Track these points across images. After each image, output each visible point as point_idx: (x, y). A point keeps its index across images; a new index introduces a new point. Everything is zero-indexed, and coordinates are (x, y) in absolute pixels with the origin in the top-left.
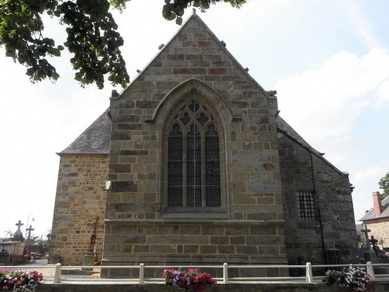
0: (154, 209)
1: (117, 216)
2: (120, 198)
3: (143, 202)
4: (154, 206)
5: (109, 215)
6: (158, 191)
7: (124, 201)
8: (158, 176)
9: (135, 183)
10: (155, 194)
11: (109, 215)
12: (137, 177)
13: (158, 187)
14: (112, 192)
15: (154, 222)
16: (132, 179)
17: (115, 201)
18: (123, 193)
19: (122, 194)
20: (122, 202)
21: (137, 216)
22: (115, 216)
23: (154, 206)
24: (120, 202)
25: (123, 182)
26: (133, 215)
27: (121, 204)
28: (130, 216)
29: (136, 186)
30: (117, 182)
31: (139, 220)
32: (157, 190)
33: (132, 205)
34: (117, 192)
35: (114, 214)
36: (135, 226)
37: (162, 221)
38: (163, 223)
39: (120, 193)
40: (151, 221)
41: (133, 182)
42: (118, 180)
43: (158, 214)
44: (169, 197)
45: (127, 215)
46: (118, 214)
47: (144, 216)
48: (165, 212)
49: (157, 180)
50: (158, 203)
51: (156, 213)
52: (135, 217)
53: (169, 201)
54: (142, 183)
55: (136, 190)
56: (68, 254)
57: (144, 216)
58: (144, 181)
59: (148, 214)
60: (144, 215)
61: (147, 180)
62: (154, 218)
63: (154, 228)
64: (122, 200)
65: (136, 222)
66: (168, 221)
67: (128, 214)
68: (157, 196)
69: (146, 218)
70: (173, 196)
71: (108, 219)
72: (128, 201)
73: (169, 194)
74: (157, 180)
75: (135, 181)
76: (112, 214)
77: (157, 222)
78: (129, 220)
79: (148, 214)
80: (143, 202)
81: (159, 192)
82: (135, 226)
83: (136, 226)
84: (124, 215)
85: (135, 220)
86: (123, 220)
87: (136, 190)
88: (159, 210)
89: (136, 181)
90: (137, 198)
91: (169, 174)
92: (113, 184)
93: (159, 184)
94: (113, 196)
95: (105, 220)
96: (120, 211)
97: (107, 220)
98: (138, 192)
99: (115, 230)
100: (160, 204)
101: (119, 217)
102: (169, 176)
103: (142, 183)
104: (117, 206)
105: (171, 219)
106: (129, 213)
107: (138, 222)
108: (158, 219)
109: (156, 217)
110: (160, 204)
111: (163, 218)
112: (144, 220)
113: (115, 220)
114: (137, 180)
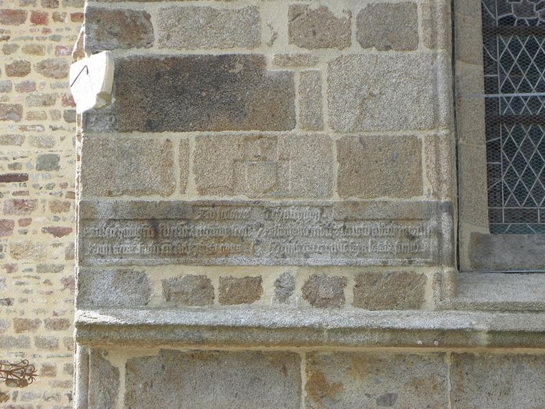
0: (409, 246)
1: (158, 290)
2: (177, 171)
3: (336, 198)
4: (409, 226)
5: (103, 284)
6: (435, 124)
7: (202, 191)
8: (431, 22)
9: (271, 69)
10: (416, 143)
11: (103, 284)
12: (282, 26)
13: (435, 98)
14: (113, 128)
15: (420, 331)
16: (256, 44)
17: (143, 192)
18: (192, 135)
19: (185, 145)
20: (192, 196)
21: (298, 292)
22: (147, 293)
23: (409, 226)
24: (176, 197)
25: (189, 59)
26: (269, 288)
27: (184, 213)
28: (248, 290)
29: (283, 87)
30: (151, 61)
31: (315, 317)
32: (430, 121)
33: (258, 216)
34: (151, 127)
35: (142, 279)
36: (284, 362)
37: (480, 322)
38: (484, 339)
39: (176, 137)
40: (400, 324)
41: (260, 61)
42: (155, 51)
43: (439, 280)
44: (492, 172)
45: (224, 282)
46: (161, 274)
47: (349, 293)
48: (478, 267)
49: (422, 48)
50: (439, 207)
51: (430, 273)
52: (284, 292)
53: (494, 196)
54: (322, 68)
55: (280, 117)
56: (162, 351)
57: (349, 293)
58: (332, 54)
59: (367, 279)
60: (342, 283)
61: (356, 48)
62: (417, 304)
63: (421, 371)
64: (192, 185)
65: (292, 329)
66: (511, 322)
67: (238, 274)
68: (427, 156)
69: (355, 304)
70: (519, 163)
71: (103, 307)
72: (231, 191)
73: (492, 149)
74: (422, 48)
75: (270, 56)
76: (122, 275)
77: (441, 332)
78: (242, 315)
79: (367, 279)
80: (336, 198)
81: (443, 132)
82: (284, 362)
83: (294, 357)
84: (205, 285)
85: (285, 318)
86: (206, 317)
87: (280, 117)
88: (447, 246)
89: (286, 60)
90: (290, 168)
91: (486, 19)
92: (122, 74)
93: (440, 22)
94: (124, 154)
95: (79, 315)
96: (178, 255)
97: (95, 317)
98: (297, 131)
99: (149, 385)
100: (449, 208)
101: (174, 295)
102: (489, 33)
103: (322, 68)
104: (153, 221)
105: (437, 153)
106: (241, 266)
107: (311, 329)
108: (440, 309)
109: (430, 294)
110: (449, 208)
111: (478, 307)
112: (348, 315)
113: (143, 316)
114: (283, 45)
